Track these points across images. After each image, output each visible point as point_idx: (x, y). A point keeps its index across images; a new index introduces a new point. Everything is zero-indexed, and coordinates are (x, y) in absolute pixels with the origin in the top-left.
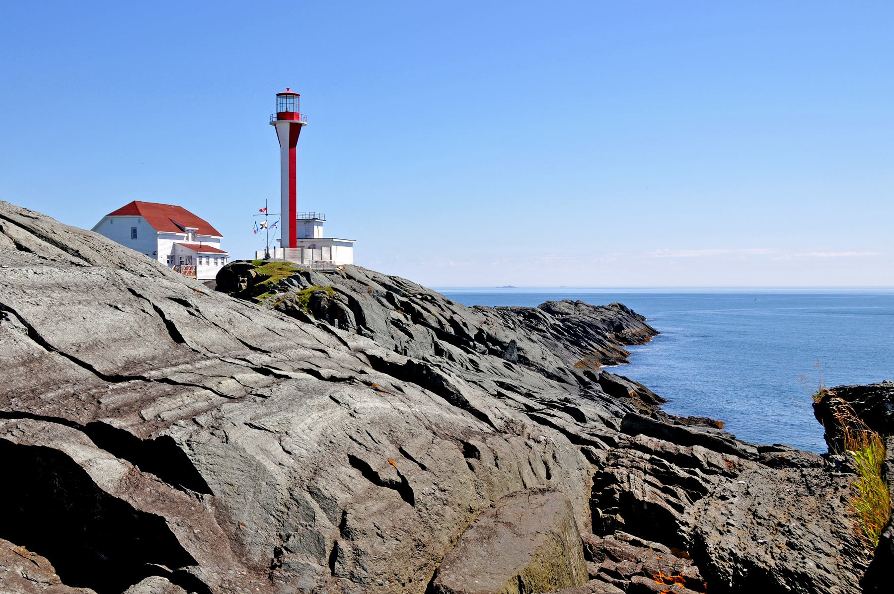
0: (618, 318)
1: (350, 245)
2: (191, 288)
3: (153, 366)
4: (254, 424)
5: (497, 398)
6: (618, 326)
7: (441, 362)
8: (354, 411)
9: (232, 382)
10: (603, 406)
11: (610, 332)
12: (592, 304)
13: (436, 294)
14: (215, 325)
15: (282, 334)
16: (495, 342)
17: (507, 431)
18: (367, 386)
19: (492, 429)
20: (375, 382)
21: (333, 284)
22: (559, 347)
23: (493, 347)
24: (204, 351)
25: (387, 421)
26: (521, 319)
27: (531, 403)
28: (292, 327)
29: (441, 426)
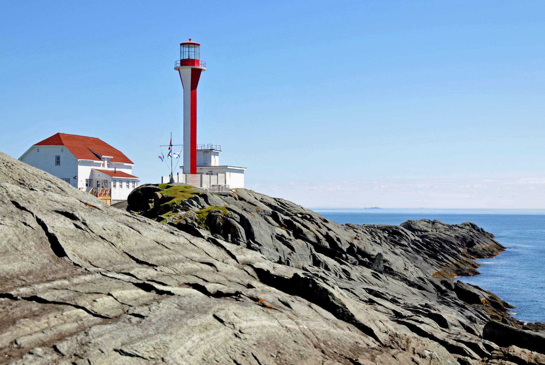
0: (470, 235)
1: (242, 172)
2: (83, 202)
3: (26, 282)
4: (125, 350)
5: (369, 304)
6: (469, 242)
7: (318, 272)
8: (240, 331)
9: (108, 300)
10: (458, 311)
11: (463, 247)
12: (447, 223)
13: (314, 214)
14: (102, 238)
15: (171, 248)
16: (365, 254)
17: (393, 346)
18: (254, 302)
19: (378, 343)
20: (262, 298)
21: (227, 204)
22: (419, 260)
23: (362, 259)
24: (86, 265)
25: (274, 341)
26: (386, 235)
27: (399, 309)
28: (182, 240)
29: (330, 343)
